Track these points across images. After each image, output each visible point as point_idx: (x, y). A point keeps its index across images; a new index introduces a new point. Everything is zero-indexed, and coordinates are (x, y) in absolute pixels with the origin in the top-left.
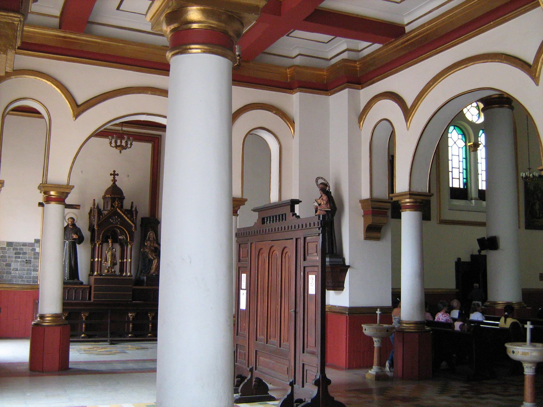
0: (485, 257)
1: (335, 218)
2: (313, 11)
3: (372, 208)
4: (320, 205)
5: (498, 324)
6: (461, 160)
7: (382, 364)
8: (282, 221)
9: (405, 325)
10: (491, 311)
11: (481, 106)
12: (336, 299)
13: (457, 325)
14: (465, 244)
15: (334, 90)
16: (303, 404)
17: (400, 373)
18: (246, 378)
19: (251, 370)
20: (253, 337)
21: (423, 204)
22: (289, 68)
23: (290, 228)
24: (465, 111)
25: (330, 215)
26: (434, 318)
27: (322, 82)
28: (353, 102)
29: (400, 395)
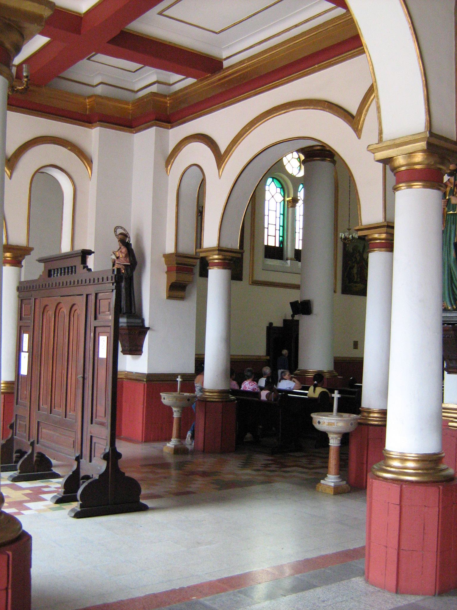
0: (298, 321)
1: (135, 274)
2: (118, 32)
3: (177, 264)
4: (118, 258)
5: (307, 393)
6: (278, 215)
7: (181, 436)
8: (72, 273)
9: (208, 394)
10: (304, 380)
11: (303, 157)
12: (131, 365)
13: (264, 395)
14: (276, 308)
15: (140, 127)
16: (90, 481)
17: (201, 446)
18: (26, 453)
19: (32, 444)
20: (35, 407)
21: (234, 263)
22: (89, 97)
23: (80, 283)
24: (285, 160)
25: (129, 270)
26: (240, 387)
27: (128, 117)
28: (160, 142)
29: (201, 470)
